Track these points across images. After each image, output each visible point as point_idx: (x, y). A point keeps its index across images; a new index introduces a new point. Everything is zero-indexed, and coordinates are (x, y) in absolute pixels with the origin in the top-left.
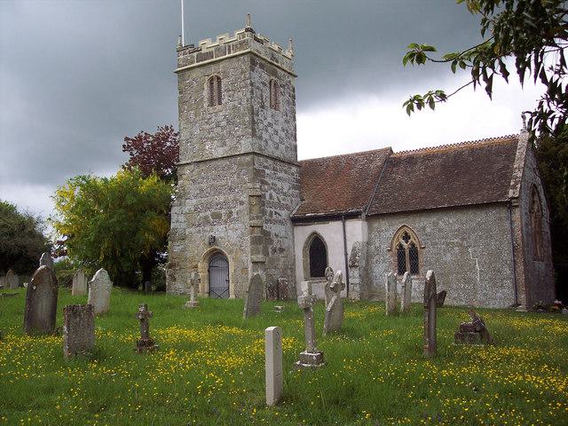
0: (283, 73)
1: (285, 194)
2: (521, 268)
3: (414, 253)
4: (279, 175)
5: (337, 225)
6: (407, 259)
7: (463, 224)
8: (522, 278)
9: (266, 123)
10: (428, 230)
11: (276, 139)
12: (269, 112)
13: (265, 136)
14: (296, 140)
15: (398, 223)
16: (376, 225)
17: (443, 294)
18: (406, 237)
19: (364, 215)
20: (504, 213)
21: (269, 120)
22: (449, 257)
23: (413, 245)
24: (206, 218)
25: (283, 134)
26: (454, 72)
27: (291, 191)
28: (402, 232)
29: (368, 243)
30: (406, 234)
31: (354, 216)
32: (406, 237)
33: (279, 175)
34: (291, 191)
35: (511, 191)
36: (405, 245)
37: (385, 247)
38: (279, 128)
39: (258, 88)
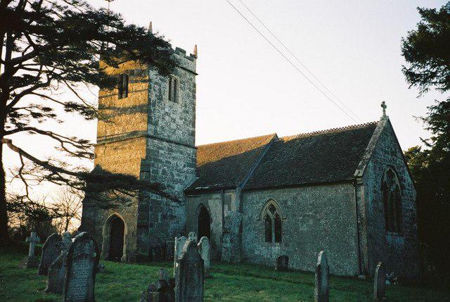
0: (183, 71)
1: (179, 171)
2: (364, 241)
3: (278, 223)
4: (174, 155)
6: (273, 229)
7: (317, 199)
8: (365, 250)
9: (162, 112)
10: (289, 203)
11: (173, 126)
12: (168, 103)
13: (161, 123)
14: (194, 126)
15: (266, 195)
17: (191, 55)
20: (351, 188)
21: (167, 110)
22: (304, 228)
23: (277, 215)
25: (181, 122)
26: (424, 13)
27: (185, 169)
28: (268, 205)
30: (272, 205)
32: (272, 208)
33: (174, 155)
34: (185, 169)
35: (357, 171)
36: (272, 216)
38: (177, 117)
39: (156, 83)
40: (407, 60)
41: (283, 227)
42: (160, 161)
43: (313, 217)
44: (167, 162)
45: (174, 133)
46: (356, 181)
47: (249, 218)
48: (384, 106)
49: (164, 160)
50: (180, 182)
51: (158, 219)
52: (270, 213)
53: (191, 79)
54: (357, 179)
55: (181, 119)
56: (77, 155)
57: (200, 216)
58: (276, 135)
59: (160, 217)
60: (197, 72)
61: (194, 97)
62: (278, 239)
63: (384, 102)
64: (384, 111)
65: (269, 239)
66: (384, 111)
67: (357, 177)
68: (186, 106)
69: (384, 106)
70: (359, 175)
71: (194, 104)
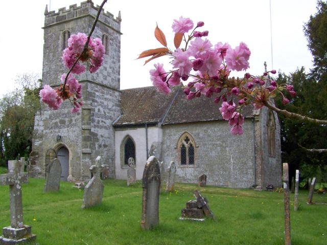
1: (110, 109)
2: (259, 162)
5: (141, 131)
14: (119, 75)
16: (168, 131)
18: (187, 140)
19: (160, 124)
22: (213, 154)
23: (191, 145)
24: (56, 123)
25: (110, 71)
27: (114, 108)
28: (184, 136)
29: (162, 143)
30: (187, 137)
31: (153, 125)
36: (186, 145)
37: (173, 146)
40: (190, 83)
41: (195, 154)
42: (96, 101)
43: (221, 146)
44: (101, 102)
45: (105, 79)
46: (253, 118)
47: (167, 147)
48: (265, 65)
49: (99, 100)
50: (111, 118)
51: (95, 148)
52: (185, 143)
53: (117, 37)
54: (256, 117)
55: (111, 68)
56: (147, 192)
57: (182, 148)
58: (311, 17)
59: (97, 146)
60: (121, 32)
61: (119, 52)
62: (192, 161)
63: (265, 62)
64: (266, 68)
65: (183, 162)
66: (266, 68)
67: (255, 116)
68: (114, 58)
69: (265, 65)
70: (257, 114)
71: (119, 57)
